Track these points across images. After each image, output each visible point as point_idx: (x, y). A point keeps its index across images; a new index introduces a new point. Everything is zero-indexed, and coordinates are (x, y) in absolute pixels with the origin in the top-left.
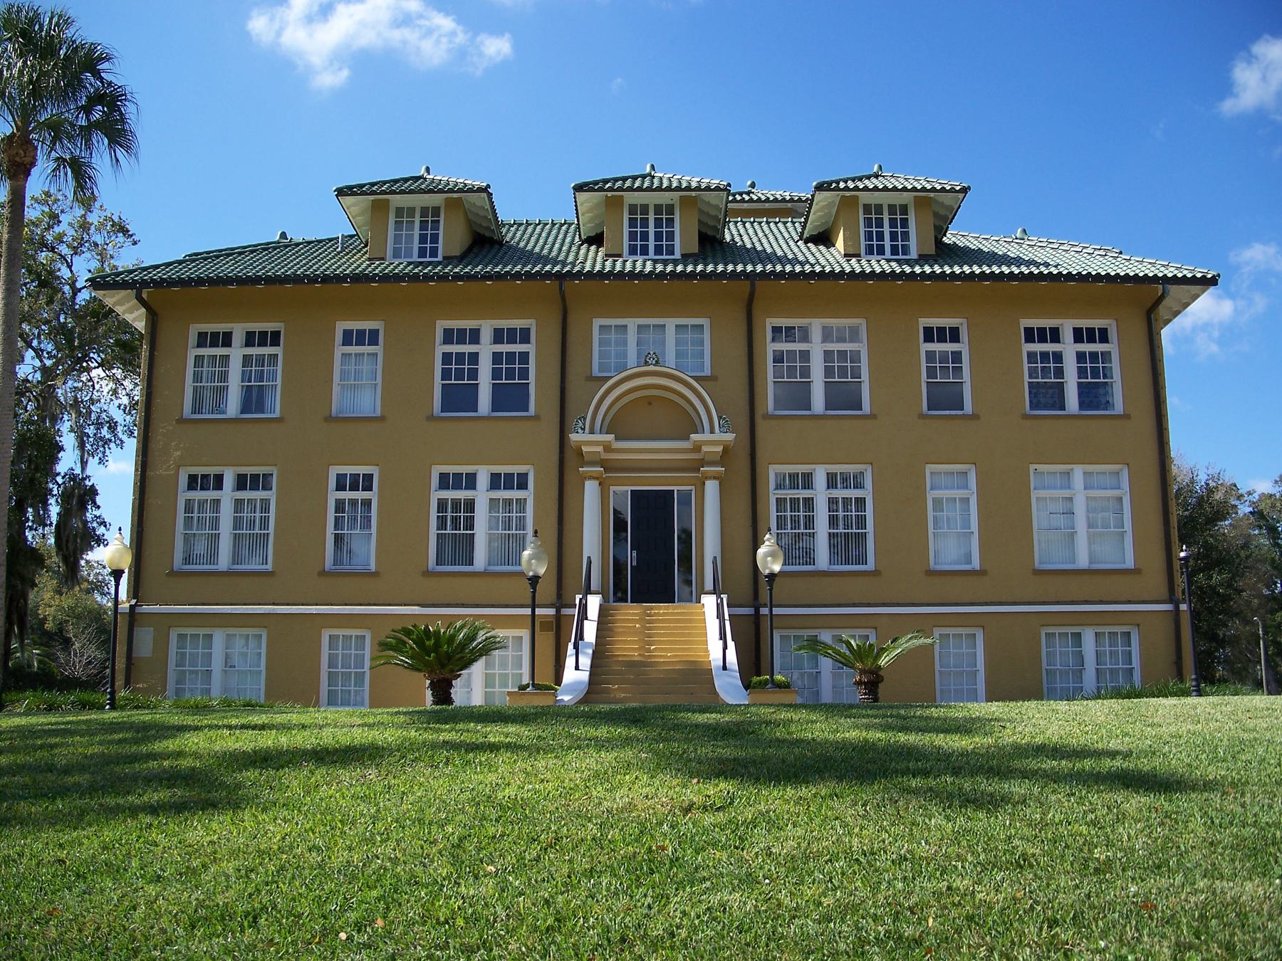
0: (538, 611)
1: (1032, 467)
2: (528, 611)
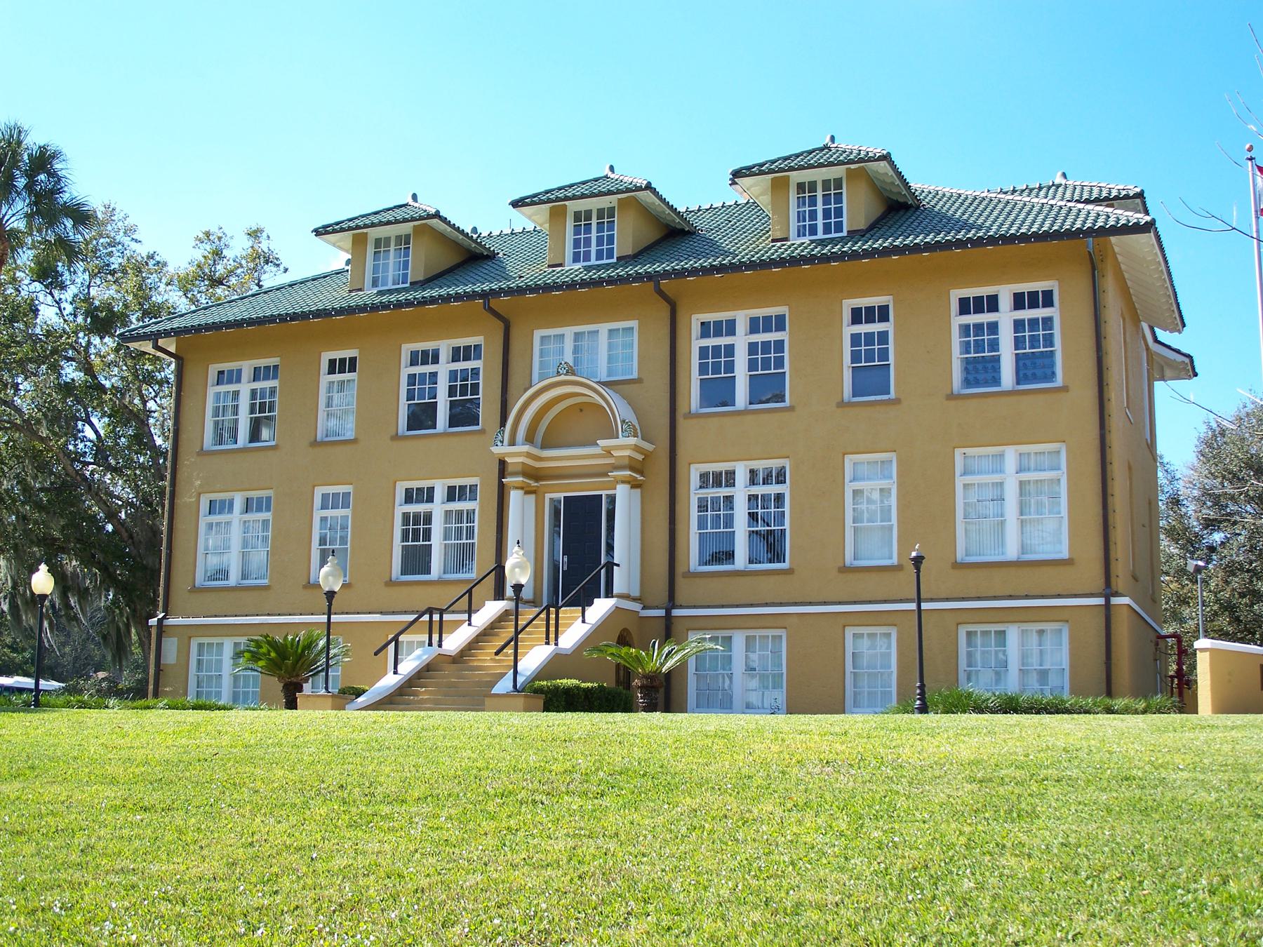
0: (924, 606)
1: (958, 452)
2: (324, 618)
